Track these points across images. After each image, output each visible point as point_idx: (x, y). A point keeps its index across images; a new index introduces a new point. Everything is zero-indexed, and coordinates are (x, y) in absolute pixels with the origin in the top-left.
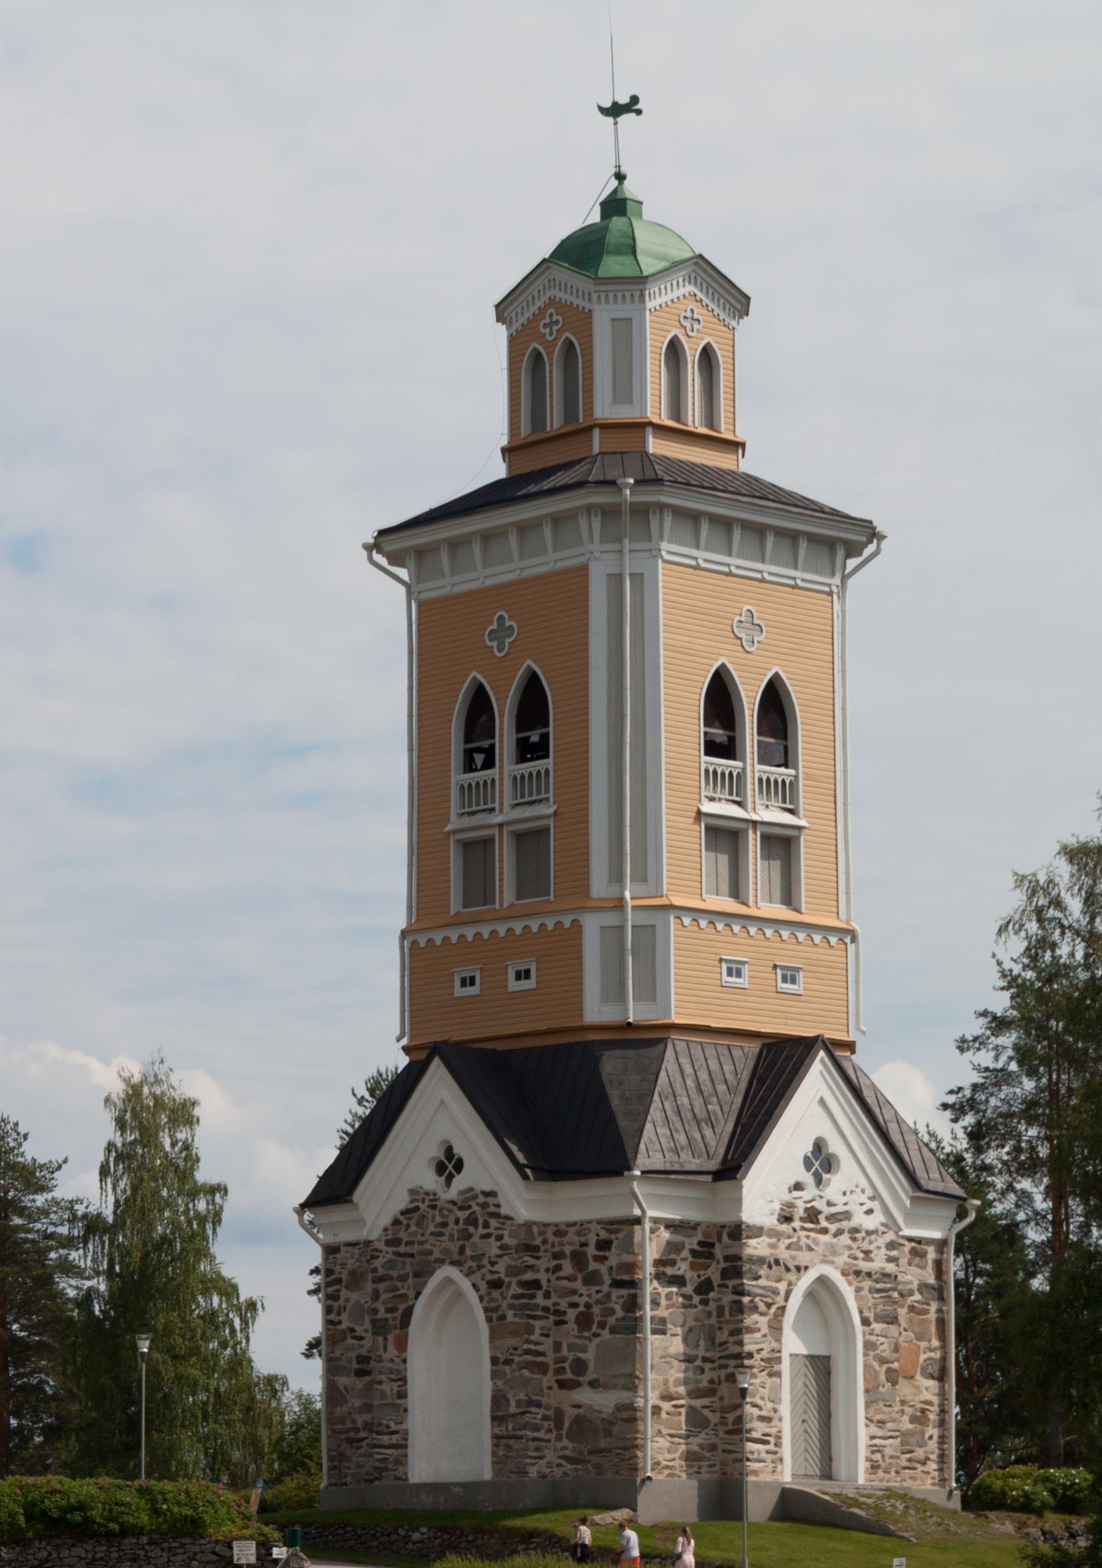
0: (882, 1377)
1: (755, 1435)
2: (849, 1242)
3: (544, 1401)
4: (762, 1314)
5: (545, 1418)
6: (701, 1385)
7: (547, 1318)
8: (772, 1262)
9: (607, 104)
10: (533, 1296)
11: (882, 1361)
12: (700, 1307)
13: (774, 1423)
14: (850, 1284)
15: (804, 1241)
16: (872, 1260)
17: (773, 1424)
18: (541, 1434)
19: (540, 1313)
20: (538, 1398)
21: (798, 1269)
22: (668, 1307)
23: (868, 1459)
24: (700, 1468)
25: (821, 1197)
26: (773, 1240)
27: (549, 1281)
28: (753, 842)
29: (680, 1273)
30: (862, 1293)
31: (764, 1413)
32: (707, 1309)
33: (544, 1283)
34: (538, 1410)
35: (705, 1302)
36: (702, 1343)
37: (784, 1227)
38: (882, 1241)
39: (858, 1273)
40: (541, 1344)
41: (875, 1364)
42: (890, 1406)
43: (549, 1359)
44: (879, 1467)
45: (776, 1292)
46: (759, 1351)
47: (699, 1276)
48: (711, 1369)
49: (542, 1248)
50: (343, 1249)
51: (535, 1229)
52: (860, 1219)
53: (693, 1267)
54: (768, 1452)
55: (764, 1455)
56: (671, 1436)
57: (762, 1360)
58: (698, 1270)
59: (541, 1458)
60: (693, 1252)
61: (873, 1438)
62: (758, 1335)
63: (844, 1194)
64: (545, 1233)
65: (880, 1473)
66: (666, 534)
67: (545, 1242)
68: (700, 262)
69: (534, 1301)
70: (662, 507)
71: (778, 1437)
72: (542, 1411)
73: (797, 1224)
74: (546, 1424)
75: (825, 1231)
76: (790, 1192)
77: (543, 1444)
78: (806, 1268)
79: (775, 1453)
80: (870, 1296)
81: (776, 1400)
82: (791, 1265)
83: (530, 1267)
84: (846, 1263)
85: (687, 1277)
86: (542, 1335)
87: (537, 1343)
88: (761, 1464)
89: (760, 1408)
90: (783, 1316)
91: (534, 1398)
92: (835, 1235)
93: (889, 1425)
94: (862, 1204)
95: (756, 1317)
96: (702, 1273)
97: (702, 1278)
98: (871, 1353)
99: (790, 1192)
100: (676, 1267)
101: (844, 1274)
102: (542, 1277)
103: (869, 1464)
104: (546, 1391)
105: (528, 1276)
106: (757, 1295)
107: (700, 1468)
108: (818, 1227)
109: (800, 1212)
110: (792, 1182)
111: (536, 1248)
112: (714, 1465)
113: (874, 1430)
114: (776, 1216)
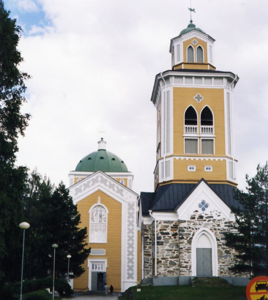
0: (224, 252)
1: (183, 266)
2: (213, 223)
3: (149, 262)
4: (185, 239)
5: (149, 265)
6: (174, 256)
7: (150, 244)
8: (188, 228)
9: (190, 8)
10: (147, 240)
11: (223, 249)
12: (174, 239)
13: (189, 263)
14: (213, 232)
15: (198, 223)
16: (220, 226)
17: (188, 263)
18: (148, 269)
19: (148, 243)
20: (148, 261)
21: (196, 229)
22: (164, 239)
23: (219, 271)
24: (173, 274)
25: (203, 213)
26: (189, 223)
27: (151, 237)
28: (199, 143)
29: (168, 232)
30: (217, 234)
31: (186, 261)
32: (176, 239)
33: (150, 237)
34: (147, 264)
35: (175, 238)
36: (174, 247)
37: (193, 220)
38: (223, 222)
39: (215, 229)
40: (148, 250)
41: (222, 250)
42: (226, 258)
43: (151, 253)
44: (223, 272)
45: (190, 234)
46: (184, 247)
47: (173, 232)
48: (177, 252)
49: (149, 230)
50: (153, 237)
51: (147, 226)
52: (215, 217)
53: (171, 230)
54: (187, 270)
55: (186, 270)
56: (165, 267)
57: (185, 249)
58: (173, 231)
59: (148, 274)
60: (172, 227)
61: (221, 266)
62: (184, 244)
63: (211, 212)
64: (150, 227)
65: (223, 274)
66: (173, 82)
67: (150, 229)
68: (195, 30)
69: (147, 241)
70: (171, 76)
71: (190, 266)
72: (149, 264)
73: (196, 219)
74: (150, 267)
75: (205, 220)
76: (194, 212)
77: (149, 271)
78: (199, 229)
79: (189, 270)
80: (219, 234)
81: (190, 257)
82: (194, 228)
83: (146, 234)
84: (211, 227)
85: (170, 233)
86: (149, 248)
87: (147, 250)
88: (185, 273)
89: (185, 260)
90: (192, 239)
91: (146, 261)
92: (208, 221)
93: (226, 263)
94: (216, 214)
95: (183, 240)
96: (174, 232)
97: (174, 233)
98: (220, 247)
99: (194, 212)
100: (167, 231)
101: (211, 230)
102: (149, 236)
103: (219, 272)
104: (150, 260)
105: (146, 236)
106: (183, 235)
107: (173, 274)
108: (203, 220)
109: (197, 217)
110: (195, 210)
111: (148, 230)
112: (178, 273)
113: (221, 264)
114: (190, 217)
